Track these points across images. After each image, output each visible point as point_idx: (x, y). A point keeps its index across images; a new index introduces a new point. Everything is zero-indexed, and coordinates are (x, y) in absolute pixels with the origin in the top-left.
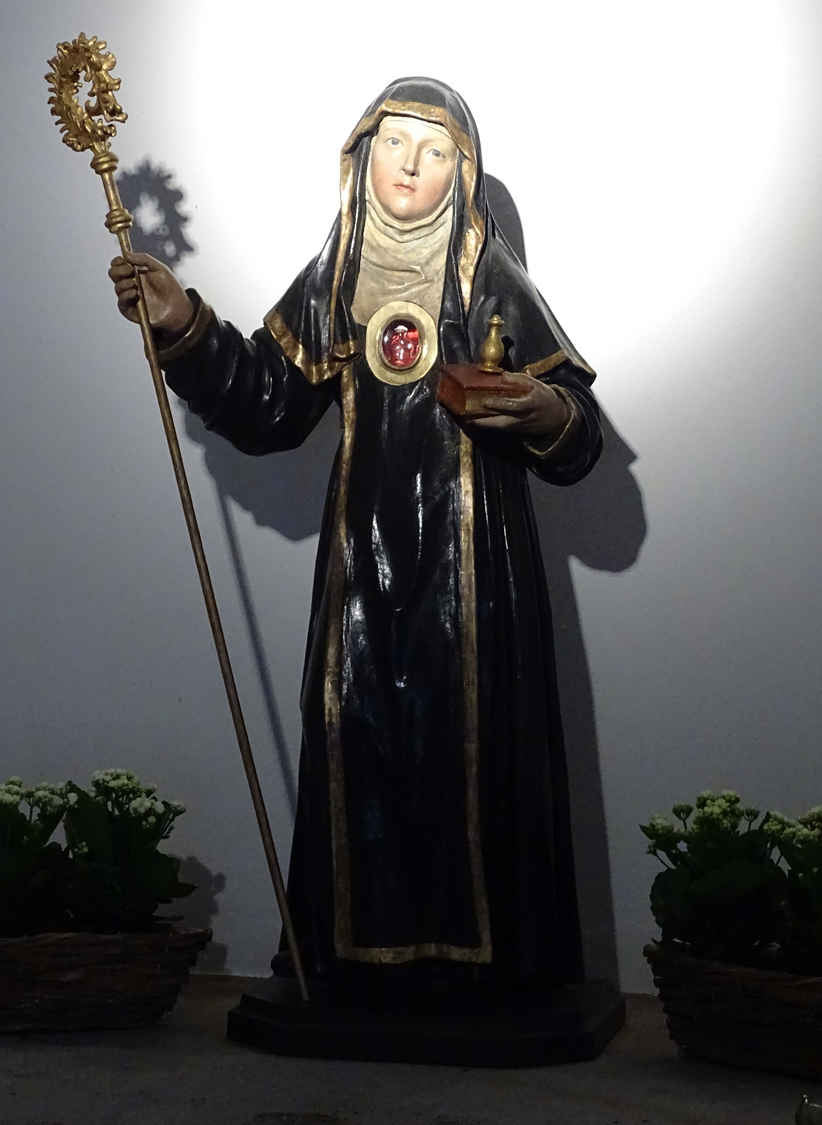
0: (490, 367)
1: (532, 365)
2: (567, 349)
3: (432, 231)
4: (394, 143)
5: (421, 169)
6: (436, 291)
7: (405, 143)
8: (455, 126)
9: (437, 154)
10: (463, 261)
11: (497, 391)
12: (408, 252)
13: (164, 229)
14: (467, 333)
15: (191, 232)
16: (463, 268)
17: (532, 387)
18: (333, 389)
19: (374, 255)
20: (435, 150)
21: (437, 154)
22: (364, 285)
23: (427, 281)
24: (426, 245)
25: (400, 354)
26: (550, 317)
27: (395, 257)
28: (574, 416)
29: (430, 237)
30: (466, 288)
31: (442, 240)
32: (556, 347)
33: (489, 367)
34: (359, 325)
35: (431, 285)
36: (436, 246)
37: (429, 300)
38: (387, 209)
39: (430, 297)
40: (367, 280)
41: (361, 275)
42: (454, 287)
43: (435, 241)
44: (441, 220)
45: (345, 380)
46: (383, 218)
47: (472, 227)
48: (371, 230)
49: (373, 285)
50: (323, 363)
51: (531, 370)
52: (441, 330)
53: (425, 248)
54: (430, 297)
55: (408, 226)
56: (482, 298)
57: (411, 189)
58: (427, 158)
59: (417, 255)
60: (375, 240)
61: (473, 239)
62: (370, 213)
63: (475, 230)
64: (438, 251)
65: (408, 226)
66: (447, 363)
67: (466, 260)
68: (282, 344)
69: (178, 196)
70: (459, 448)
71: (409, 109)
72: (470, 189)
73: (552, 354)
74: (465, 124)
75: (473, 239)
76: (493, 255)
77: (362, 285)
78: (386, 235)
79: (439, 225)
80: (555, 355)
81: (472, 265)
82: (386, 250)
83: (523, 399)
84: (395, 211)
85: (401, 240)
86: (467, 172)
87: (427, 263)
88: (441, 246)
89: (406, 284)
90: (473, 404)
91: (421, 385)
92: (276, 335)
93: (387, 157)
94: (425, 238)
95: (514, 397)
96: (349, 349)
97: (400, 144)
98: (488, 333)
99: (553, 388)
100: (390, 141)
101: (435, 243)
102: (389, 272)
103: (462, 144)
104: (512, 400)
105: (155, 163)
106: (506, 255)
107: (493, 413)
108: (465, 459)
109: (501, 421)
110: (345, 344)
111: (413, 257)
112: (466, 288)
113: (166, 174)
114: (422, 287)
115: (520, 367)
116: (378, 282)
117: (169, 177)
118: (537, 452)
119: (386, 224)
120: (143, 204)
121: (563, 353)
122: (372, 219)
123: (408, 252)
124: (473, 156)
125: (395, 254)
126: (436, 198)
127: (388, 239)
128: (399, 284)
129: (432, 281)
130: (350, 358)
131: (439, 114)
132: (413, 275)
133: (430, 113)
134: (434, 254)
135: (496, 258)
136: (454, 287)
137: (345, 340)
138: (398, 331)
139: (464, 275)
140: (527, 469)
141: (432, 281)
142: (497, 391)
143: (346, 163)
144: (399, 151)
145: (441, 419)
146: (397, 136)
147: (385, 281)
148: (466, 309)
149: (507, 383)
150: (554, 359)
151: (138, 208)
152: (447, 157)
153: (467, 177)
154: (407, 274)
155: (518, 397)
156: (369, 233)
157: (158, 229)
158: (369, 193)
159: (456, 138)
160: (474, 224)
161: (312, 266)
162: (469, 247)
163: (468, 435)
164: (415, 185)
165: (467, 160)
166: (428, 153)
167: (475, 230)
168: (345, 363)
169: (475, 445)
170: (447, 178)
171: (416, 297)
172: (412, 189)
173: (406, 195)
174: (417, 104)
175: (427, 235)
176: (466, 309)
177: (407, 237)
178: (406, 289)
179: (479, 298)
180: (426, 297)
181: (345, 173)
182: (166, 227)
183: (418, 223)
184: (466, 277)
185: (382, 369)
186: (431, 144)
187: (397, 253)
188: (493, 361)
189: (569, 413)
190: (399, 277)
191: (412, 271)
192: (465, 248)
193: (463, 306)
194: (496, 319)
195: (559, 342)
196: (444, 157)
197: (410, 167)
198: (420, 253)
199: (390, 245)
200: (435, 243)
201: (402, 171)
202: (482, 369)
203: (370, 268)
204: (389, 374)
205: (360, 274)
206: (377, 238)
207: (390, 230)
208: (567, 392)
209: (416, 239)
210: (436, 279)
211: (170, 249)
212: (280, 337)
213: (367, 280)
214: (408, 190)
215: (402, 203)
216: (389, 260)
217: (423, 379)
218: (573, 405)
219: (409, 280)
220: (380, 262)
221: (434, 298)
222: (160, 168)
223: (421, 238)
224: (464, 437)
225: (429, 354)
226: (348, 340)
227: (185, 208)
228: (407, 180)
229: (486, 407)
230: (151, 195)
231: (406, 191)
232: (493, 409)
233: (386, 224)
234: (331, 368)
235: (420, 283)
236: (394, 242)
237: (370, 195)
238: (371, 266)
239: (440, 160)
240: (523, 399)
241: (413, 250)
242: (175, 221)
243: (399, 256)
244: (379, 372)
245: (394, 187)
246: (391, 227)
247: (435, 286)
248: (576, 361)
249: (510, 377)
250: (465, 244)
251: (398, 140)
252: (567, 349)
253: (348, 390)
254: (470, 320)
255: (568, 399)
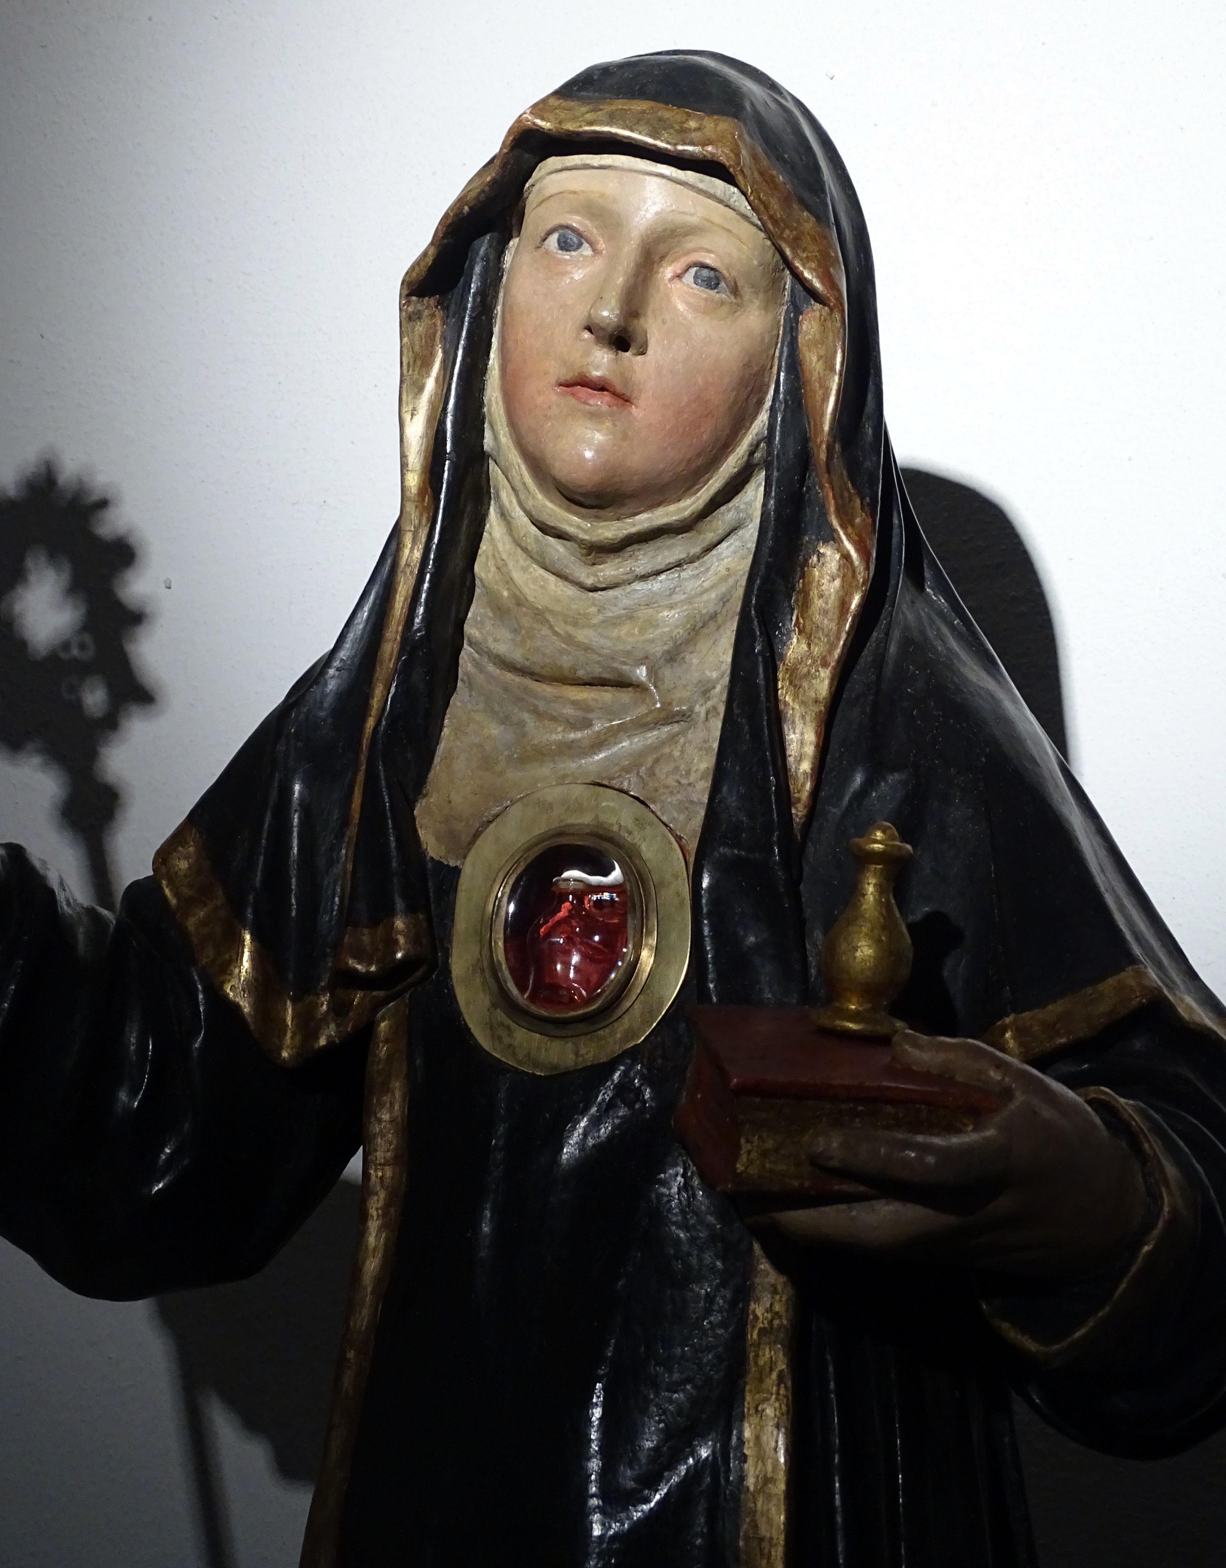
0: (854, 1017)
1: (1027, 1014)
2: (1159, 965)
3: (696, 550)
4: (565, 245)
5: (653, 329)
6: (697, 752)
7: (601, 245)
8: (770, 181)
9: (711, 277)
10: (795, 648)
11: (869, 1103)
12: (615, 622)
13: (82, 647)
14: (796, 897)
15: (153, 653)
16: (792, 671)
17: (1007, 1094)
18: (338, 1083)
19: (505, 634)
20: (704, 266)
21: (711, 277)
22: (468, 730)
23: (669, 717)
24: (677, 598)
25: (567, 965)
26: (1103, 853)
27: (569, 639)
28: (1174, 1211)
29: (688, 572)
30: (801, 740)
31: (731, 581)
32: (1119, 955)
33: (852, 1015)
34: (438, 864)
35: (682, 733)
36: (708, 602)
37: (671, 781)
38: (538, 466)
39: (676, 769)
40: (478, 717)
41: (460, 700)
42: (756, 734)
43: (706, 585)
44: (727, 515)
45: (383, 1050)
46: (529, 504)
47: (837, 540)
48: (502, 551)
49: (495, 730)
50: (318, 995)
51: (1021, 1032)
52: (705, 883)
53: (671, 607)
54: (676, 769)
55: (610, 530)
56: (858, 779)
57: (615, 394)
58: (677, 295)
59: (642, 630)
60: (509, 581)
61: (833, 572)
62: (498, 497)
63: (840, 548)
64: (713, 617)
65: (610, 530)
66: (720, 1000)
67: (805, 647)
68: (191, 923)
69: (122, 554)
70: (745, 1312)
71: (612, 119)
72: (825, 399)
73: (1103, 977)
74: (818, 187)
75: (833, 572)
76: (907, 642)
77: (458, 731)
78: (546, 569)
79: (721, 532)
80: (1111, 981)
81: (825, 664)
82: (540, 615)
83: (968, 1138)
84: (561, 469)
85: (589, 581)
86: (814, 343)
87: (673, 656)
88: (724, 600)
89: (598, 727)
90: (764, 1154)
91: (625, 1074)
92: (176, 894)
93: (549, 294)
94: (673, 575)
95: (930, 1128)
96: (391, 945)
97: (586, 250)
98: (854, 890)
99: (1090, 1102)
100: (554, 238)
101: (706, 591)
102: (548, 690)
103: (795, 244)
104: (920, 1138)
105: (70, 467)
106: (954, 644)
107: (847, 1187)
108: (766, 1354)
109: (881, 1219)
110: (380, 931)
111: (628, 636)
112: (801, 740)
113: (95, 498)
114: (652, 736)
115: (985, 1026)
116: (505, 721)
117: (103, 504)
118: (1031, 1345)
119: (545, 529)
120: (33, 578)
121: (1141, 975)
122: (504, 514)
123: (615, 622)
124: (833, 285)
125: (570, 629)
126: (706, 433)
127: (552, 578)
128: (573, 726)
129: (684, 717)
130: (392, 977)
131: (714, 137)
132: (625, 696)
133: (683, 131)
134: (698, 628)
135: (916, 647)
136: (756, 734)
137: (381, 914)
138: (563, 885)
139: (796, 696)
140: (1014, 1394)
141: (684, 717)
142: (869, 1103)
143: (420, 328)
144: (580, 271)
145: (688, 1208)
146: (575, 221)
147: (526, 716)
148: (799, 812)
149: (907, 1072)
150: (1107, 997)
151: (20, 590)
152: (747, 292)
153: (812, 360)
154: (607, 695)
155: (951, 1129)
156: (491, 563)
157: (66, 646)
158: (492, 426)
159: (775, 222)
160: (835, 523)
161: (313, 676)
162: (818, 603)
163: (779, 1266)
164: (626, 381)
165: (817, 306)
166: (679, 276)
167: (840, 548)
168: (380, 994)
169: (805, 1306)
170: (747, 365)
171: (627, 770)
172: (618, 394)
173: (595, 416)
174: (640, 106)
175: (679, 564)
176: (799, 812)
177: (610, 570)
178: (598, 744)
179: (847, 779)
180: (662, 771)
181: (414, 363)
182: (88, 638)
183: (645, 520)
184: (803, 703)
185: (500, 1015)
186: (691, 243)
187: (575, 624)
188: (870, 991)
189: (1155, 1198)
190: (574, 703)
191: (622, 683)
192: (806, 604)
193: (785, 798)
194: (879, 835)
195: (1128, 936)
196: (735, 291)
197: (608, 314)
198: (652, 623)
199: (557, 600)
200: (706, 591)
201: (587, 335)
202: (825, 1019)
203: (490, 676)
204: (526, 1040)
205: (455, 700)
206: (517, 576)
207: (557, 548)
208: (1147, 1118)
209: (644, 578)
210: (700, 710)
211: (95, 698)
212: (188, 904)
213: (478, 717)
214: (607, 397)
215: (586, 444)
216: (548, 648)
217: (633, 1054)
218: (1171, 1170)
219: (610, 712)
220: (517, 655)
221: (688, 773)
222: (80, 481)
223: (658, 573)
224: (767, 1274)
225: (660, 965)
226: (391, 913)
227: (138, 587)
228: (601, 362)
229: (816, 1162)
230: (53, 556)
231: (600, 402)
232: (844, 1173)
233: (545, 529)
234: (339, 1010)
235: (642, 725)
236: (571, 591)
237: (497, 436)
238: (491, 668)
239: (722, 303)
240: (968, 1138)
241: (630, 616)
242: (111, 623)
243: (583, 635)
244: (491, 1027)
245: (559, 390)
246: (561, 535)
247: (696, 735)
248: (1189, 1008)
249: (925, 1052)
250: (805, 592)
251: (579, 234)
252: (1159, 965)
253: (386, 1089)
254: (811, 849)
255: (1153, 1146)
